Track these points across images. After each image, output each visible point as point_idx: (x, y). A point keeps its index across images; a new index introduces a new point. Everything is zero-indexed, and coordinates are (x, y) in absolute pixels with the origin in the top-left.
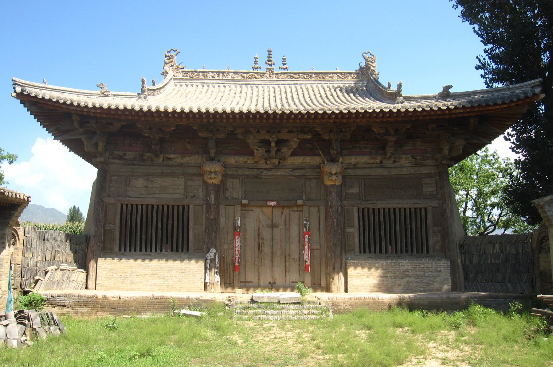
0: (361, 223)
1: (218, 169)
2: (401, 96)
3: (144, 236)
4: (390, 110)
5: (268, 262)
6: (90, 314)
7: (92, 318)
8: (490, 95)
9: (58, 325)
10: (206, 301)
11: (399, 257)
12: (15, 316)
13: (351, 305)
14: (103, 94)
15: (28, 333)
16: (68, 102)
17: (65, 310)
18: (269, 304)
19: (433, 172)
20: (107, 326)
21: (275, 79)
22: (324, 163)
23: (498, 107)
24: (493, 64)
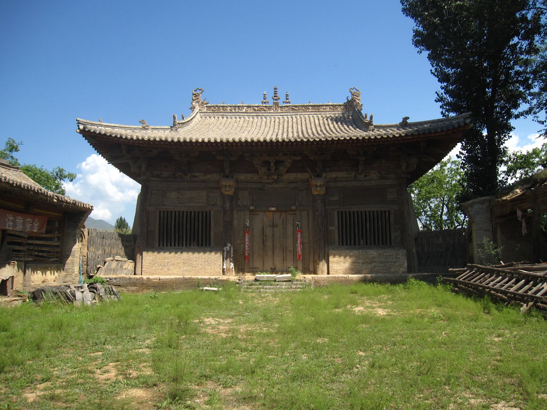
0: (340, 223)
1: (231, 183)
2: (372, 125)
3: (177, 235)
4: (357, 138)
5: (270, 253)
6: (138, 291)
7: (140, 293)
8: (435, 125)
9: (116, 295)
10: (223, 281)
11: (369, 248)
12: (88, 286)
13: (329, 282)
14: (144, 128)
15: (97, 298)
16: (119, 136)
17: (120, 289)
18: (268, 282)
19: (395, 183)
20: (151, 297)
21: (280, 111)
22: (311, 178)
23: (438, 134)
24: (448, 98)
